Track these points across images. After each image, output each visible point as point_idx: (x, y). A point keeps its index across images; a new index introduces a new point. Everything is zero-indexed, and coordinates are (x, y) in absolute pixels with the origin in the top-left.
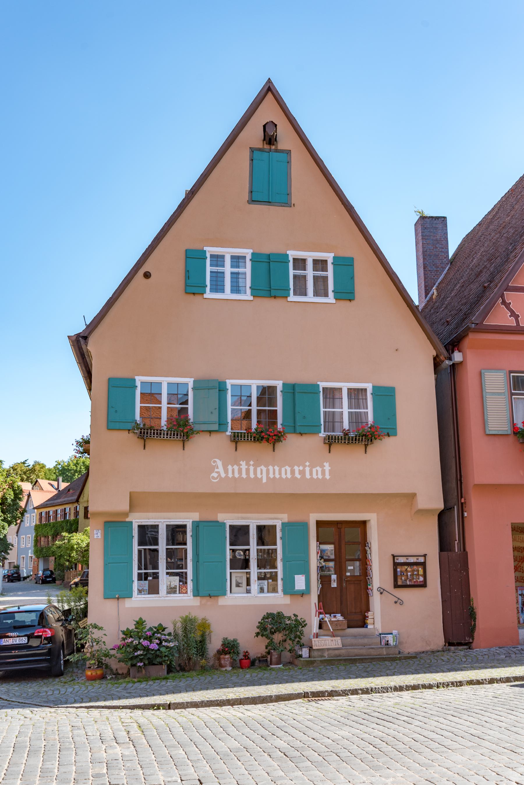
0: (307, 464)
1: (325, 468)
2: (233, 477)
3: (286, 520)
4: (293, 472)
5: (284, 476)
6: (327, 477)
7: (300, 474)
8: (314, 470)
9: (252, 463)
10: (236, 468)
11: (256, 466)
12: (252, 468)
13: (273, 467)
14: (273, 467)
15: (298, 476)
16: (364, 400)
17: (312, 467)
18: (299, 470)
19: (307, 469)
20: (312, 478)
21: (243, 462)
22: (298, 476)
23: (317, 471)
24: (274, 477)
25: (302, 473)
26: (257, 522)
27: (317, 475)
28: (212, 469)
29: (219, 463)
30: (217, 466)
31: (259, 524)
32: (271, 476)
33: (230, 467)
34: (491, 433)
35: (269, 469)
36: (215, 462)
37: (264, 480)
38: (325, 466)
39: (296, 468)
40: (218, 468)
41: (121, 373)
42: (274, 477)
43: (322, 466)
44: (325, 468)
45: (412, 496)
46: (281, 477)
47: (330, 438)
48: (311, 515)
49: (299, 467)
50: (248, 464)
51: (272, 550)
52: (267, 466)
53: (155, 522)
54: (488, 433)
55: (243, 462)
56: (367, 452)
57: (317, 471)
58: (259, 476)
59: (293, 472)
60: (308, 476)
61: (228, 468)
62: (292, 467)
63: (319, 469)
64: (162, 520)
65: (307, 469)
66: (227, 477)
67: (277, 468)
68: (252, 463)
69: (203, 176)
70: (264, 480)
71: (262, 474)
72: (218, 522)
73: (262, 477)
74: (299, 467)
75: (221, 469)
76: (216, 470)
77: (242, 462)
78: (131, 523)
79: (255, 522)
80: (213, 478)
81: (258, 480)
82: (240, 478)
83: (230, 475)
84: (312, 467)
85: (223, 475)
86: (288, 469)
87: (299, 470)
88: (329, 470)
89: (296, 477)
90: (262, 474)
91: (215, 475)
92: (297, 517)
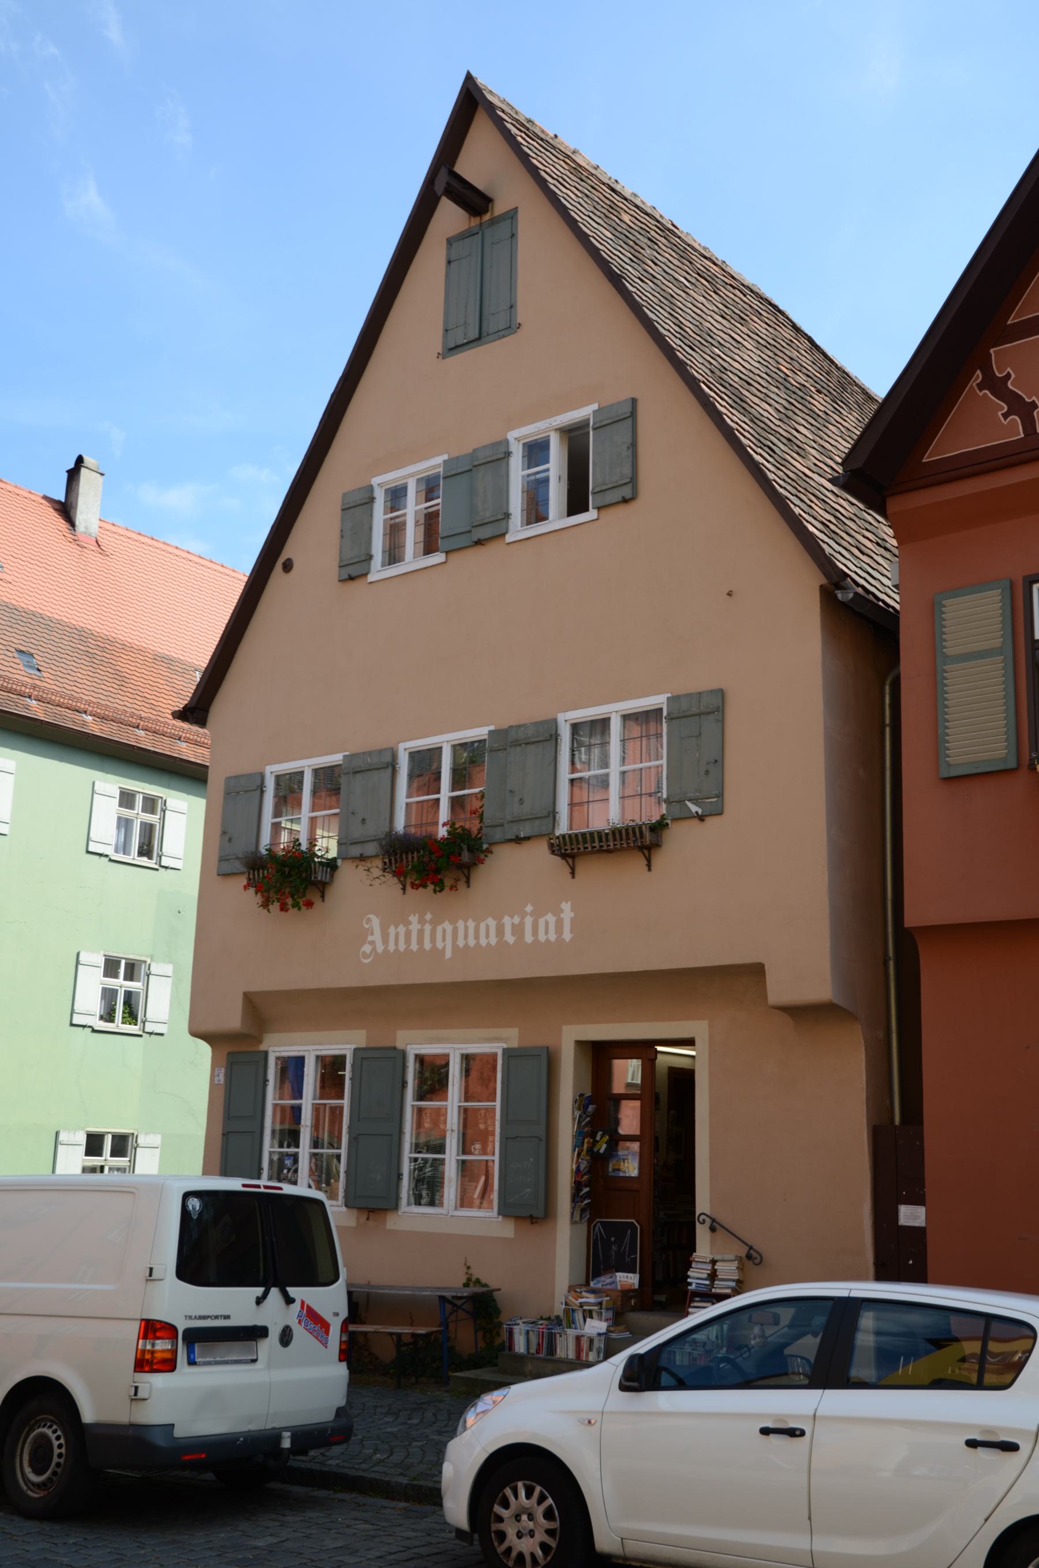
0: (529, 908)
1: (562, 916)
2: (397, 950)
3: (515, 1044)
4: (500, 931)
5: (483, 942)
6: (567, 936)
7: (513, 934)
8: (542, 922)
9: (428, 917)
10: (402, 929)
11: (435, 923)
12: (428, 928)
13: (466, 921)
14: (466, 921)
15: (510, 938)
16: (653, 740)
17: (537, 914)
18: (513, 924)
19: (529, 921)
20: (536, 941)
21: (567, 903)
22: (510, 938)
23: (444, 931)
24: (466, 946)
25: (519, 930)
26: (462, 1049)
27: (547, 933)
28: (363, 936)
29: (376, 922)
30: (372, 931)
31: (465, 1052)
32: (461, 943)
33: (392, 930)
34: (954, 773)
35: (457, 927)
36: (369, 921)
37: (448, 954)
38: (410, 923)
39: (507, 921)
40: (372, 934)
41: (244, 767)
42: (466, 946)
43: (557, 912)
44: (562, 916)
45: (757, 971)
46: (478, 944)
47: (604, 839)
48: (565, 1028)
49: (512, 917)
50: (422, 921)
51: (487, 1110)
52: (453, 922)
53: (299, 1051)
54: (946, 775)
55: (567, 903)
56: (653, 868)
57: (444, 931)
58: (439, 945)
59: (500, 931)
60: (529, 938)
61: (389, 933)
62: (499, 918)
63: (551, 918)
64: (310, 1048)
65: (529, 921)
66: (386, 951)
67: (471, 924)
68: (428, 917)
69: (334, 397)
70: (448, 954)
71: (444, 940)
72: (395, 1048)
73: (445, 945)
74: (512, 917)
75: (377, 937)
76: (370, 938)
77: (564, 903)
78: (266, 1054)
79: (458, 1049)
80: (366, 956)
81: (437, 953)
82: (408, 951)
83: (392, 948)
84: (537, 914)
85: (380, 948)
86: (492, 922)
87: (513, 924)
88: (572, 919)
89: (506, 941)
90: (444, 940)
91: (367, 948)
92: (538, 1039)
